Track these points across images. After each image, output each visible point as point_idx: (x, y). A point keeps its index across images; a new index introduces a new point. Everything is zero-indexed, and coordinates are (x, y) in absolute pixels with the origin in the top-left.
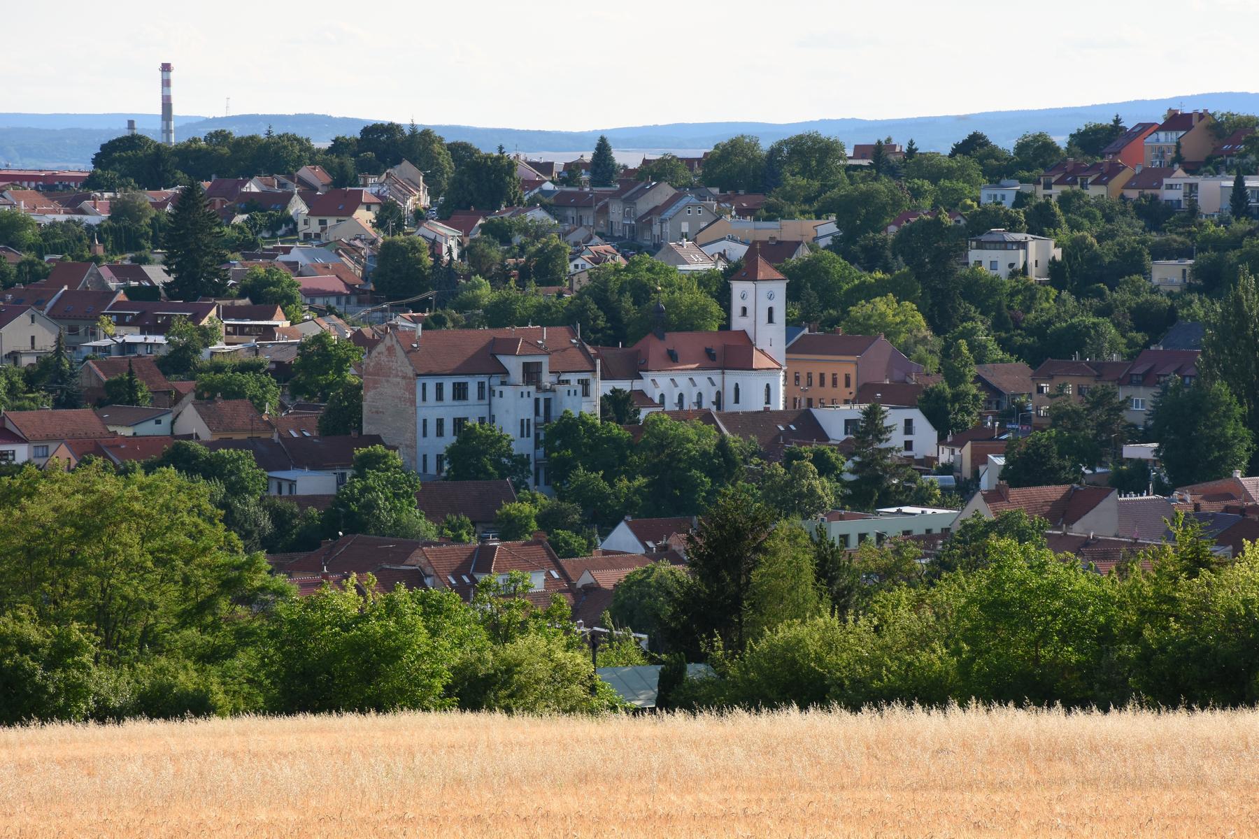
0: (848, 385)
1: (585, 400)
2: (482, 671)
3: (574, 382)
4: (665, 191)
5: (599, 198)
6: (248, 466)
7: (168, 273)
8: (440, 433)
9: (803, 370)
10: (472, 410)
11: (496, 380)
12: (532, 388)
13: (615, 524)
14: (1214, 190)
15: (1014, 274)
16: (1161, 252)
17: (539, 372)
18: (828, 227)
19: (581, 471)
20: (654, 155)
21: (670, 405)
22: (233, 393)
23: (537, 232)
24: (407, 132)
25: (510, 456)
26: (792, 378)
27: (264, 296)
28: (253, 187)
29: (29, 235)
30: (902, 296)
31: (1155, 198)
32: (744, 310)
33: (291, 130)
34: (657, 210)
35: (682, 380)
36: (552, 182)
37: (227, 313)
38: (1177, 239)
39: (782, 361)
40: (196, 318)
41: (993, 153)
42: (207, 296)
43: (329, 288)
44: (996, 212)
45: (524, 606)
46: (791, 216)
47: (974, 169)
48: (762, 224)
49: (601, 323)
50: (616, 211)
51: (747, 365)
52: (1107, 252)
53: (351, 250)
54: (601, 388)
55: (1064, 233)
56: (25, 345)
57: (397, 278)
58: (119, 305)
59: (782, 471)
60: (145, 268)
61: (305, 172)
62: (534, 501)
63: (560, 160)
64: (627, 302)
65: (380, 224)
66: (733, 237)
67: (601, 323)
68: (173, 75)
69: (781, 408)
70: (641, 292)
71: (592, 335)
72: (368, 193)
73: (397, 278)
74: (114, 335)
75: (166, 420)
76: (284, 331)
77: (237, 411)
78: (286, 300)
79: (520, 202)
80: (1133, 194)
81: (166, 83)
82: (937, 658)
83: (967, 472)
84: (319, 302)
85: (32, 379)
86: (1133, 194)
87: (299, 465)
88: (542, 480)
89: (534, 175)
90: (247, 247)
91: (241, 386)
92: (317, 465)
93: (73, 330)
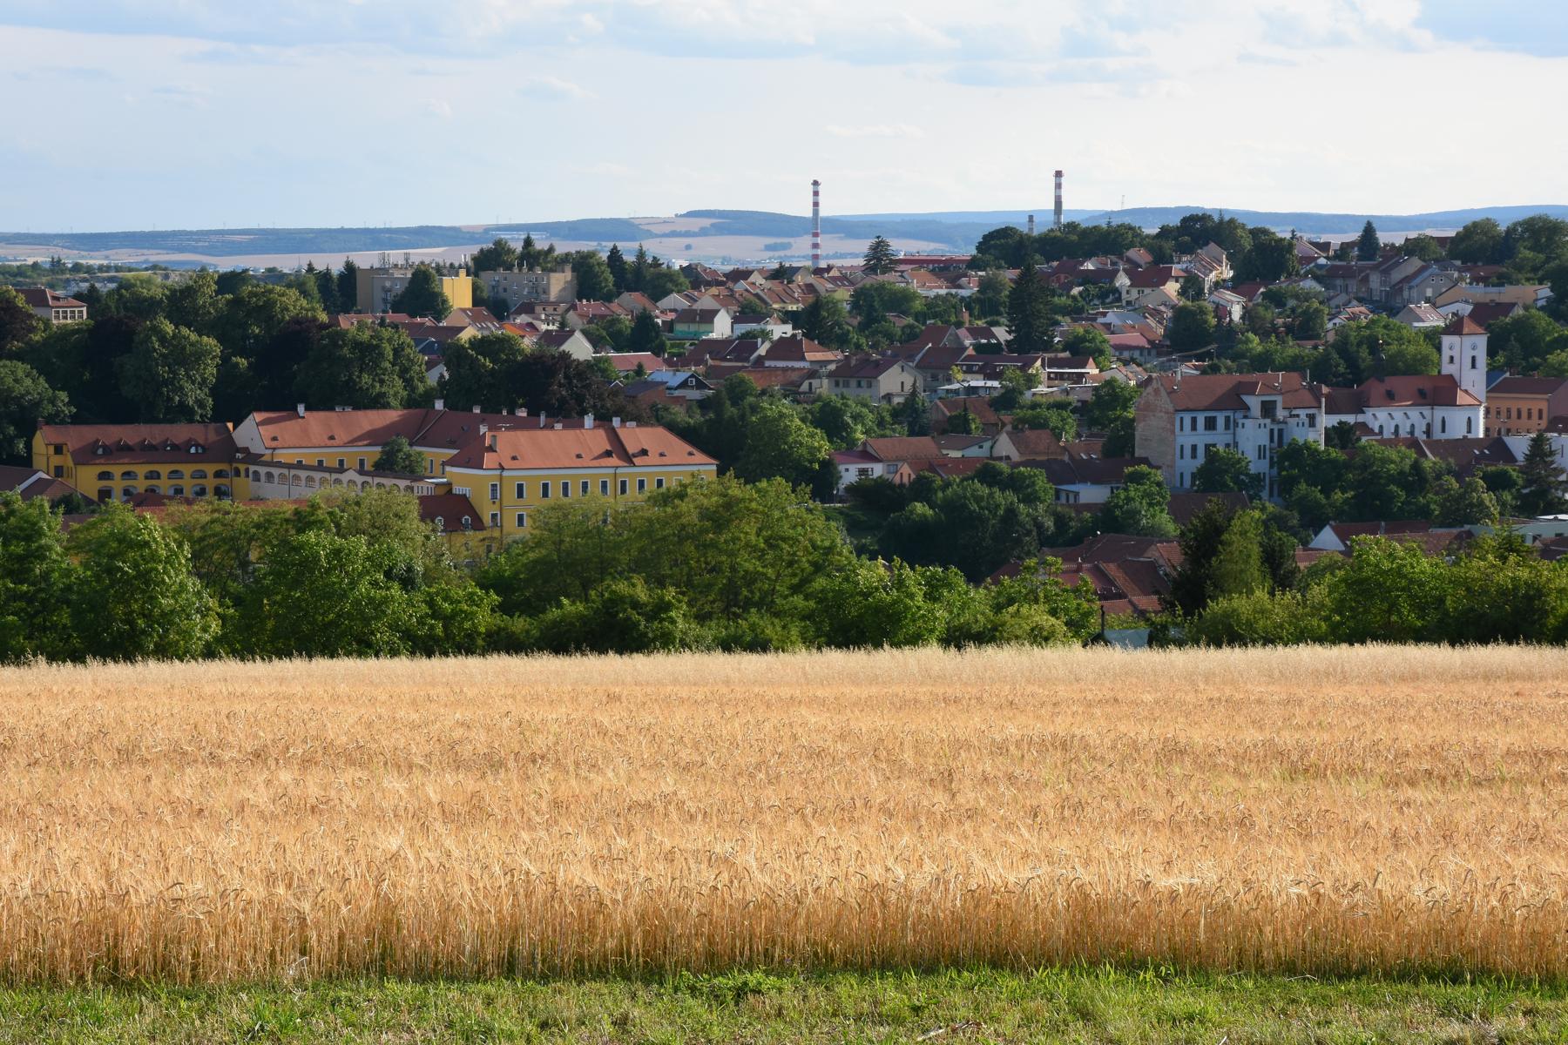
0: (1540, 418)
1: (1315, 429)
3: (1303, 417)
4: (1416, 263)
5: (1361, 270)
6: (1041, 481)
7: (1009, 332)
8: (1194, 456)
9: (1504, 406)
10: (1220, 438)
11: (1239, 415)
12: (1268, 421)
13: (1321, 528)
18: (1545, 291)
19: (1303, 486)
20: (1413, 235)
21: (1388, 434)
22: (1038, 424)
23: (1307, 297)
24: (1216, 218)
25: (1247, 475)
26: (1493, 412)
27: (1080, 350)
28: (1089, 266)
29: (918, 305)
32: (1452, 358)
33: (1127, 220)
34: (1408, 279)
35: (1398, 415)
36: (1327, 258)
37: (1052, 363)
39: (1483, 399)
40: (1024, 368)
42: (1037, 350)
43: (1134, 344)
45: (1056, 583)
46: (1518, 282)
49: (1341, 369)
50: (1375, 281)
51: (1451, 402)
53: (1156, 313)
54: (1326, 421)
56: (896, 389)
57: (1189, 334)
58: (969, 358)
60: (994, 330)
61: (1132, 253)
62: (1263, 509)
63: (1336, 240)
64: (1364, 353)
65: (1183, 292)
66: (1467, 294)
67: (1341, 369)
68: (1063, 180)
69: (1481, 435)
70: (1373, 346)
72: (1176, 269)
73: (1189, 334)
74: (963, 380)
75: (987, 445)
76: (1094, 378)
77: (1041, 439)
78: (1098, 353)
79: (1298, 274)
81: (1058, 186)
84: (1126, 355)
85: (897, 414)
87: (1083, 480)
88: (1276, 492)
89: (1315, 252)
90: (1075, 312)
91: (1046, 420)
92: (1097, 481)
93: (935, 378)
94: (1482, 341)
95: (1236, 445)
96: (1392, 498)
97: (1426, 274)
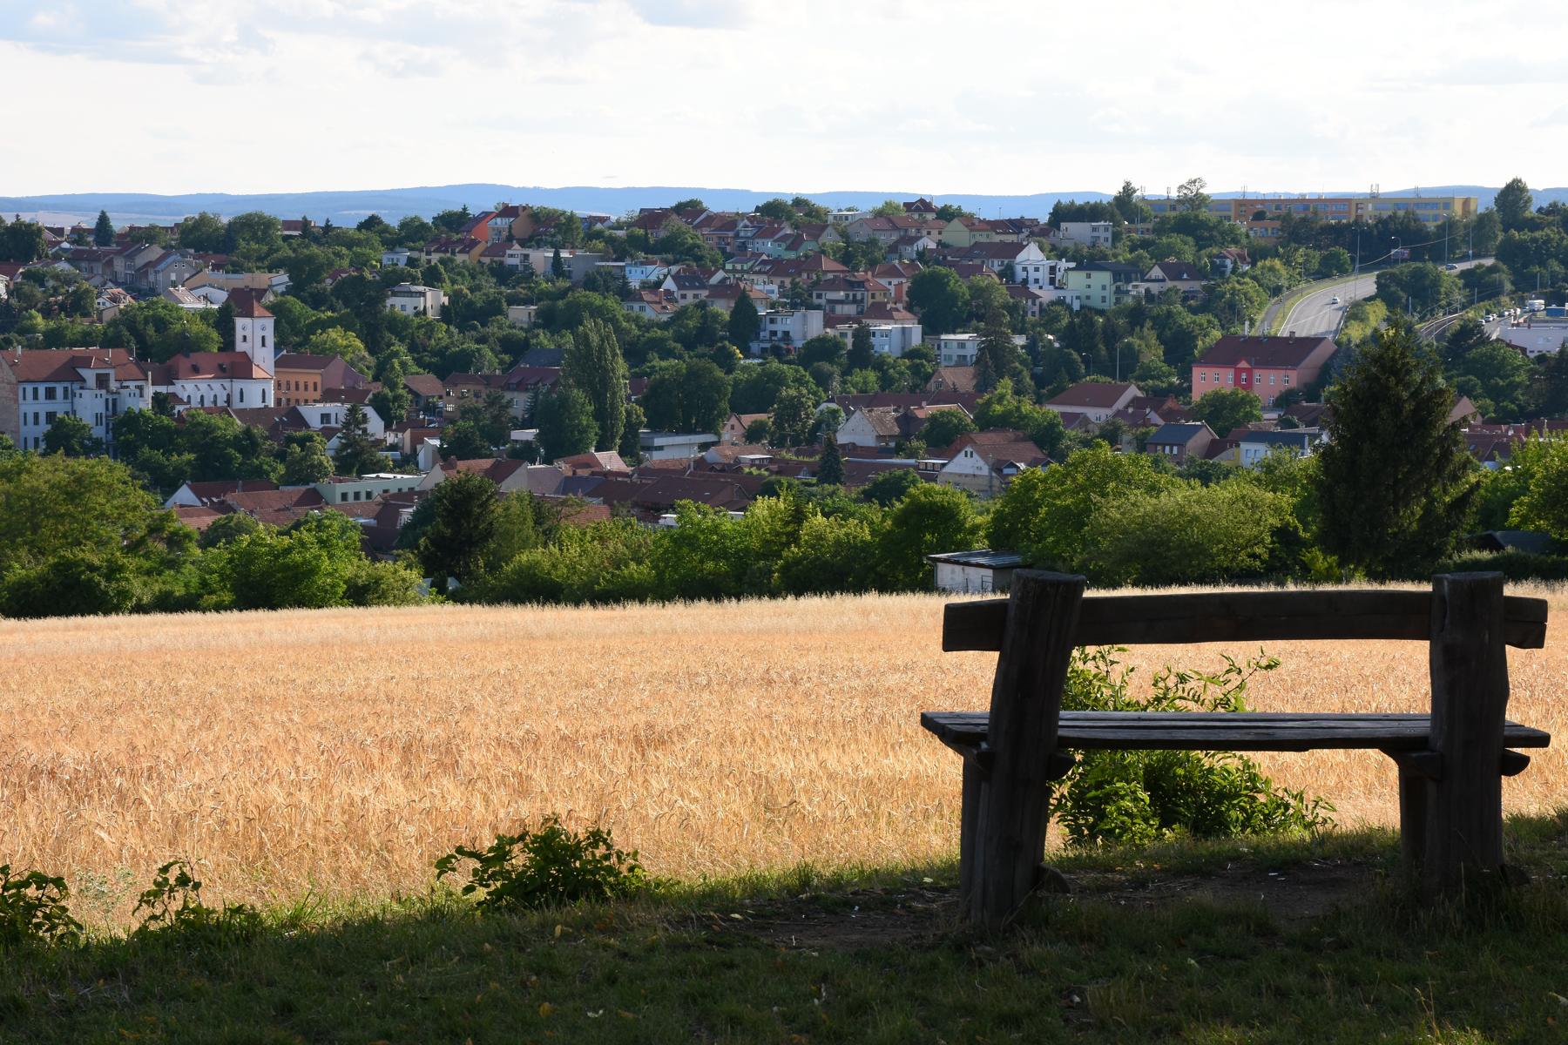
1: (141, 398)
2: (360, 582)
4: (155, 252)
5: (106, 254)
8: (36, 422)
10: (59, 407)
11: (76, 386)
14: (541, 258)
15: (417, 314)
16: (512, 301)
17: (108, 380)
18: (281, 279)
21: (195, 403)
25: (90, 439)
30: (347, 328)
31: (501, 263)
35: (203, 386)
38: (521, 291)
41: (386, 229)
44: (394, 271)
47: (376, 240)
48: (231, 276)
50: (119, 265)
52: (478, 299)
54: (150, 390)
55: (447, 285)
59: (298, 449)
64: (151, 330)
70: (161, 324)
71: (144, 353)
80: (487, 260)
82: (637, 571)
83: (407, 449)
86: (487, 260)
94: (269, 323)
95: (74, 412)
96: (230, 459)
97: (170, 260)
